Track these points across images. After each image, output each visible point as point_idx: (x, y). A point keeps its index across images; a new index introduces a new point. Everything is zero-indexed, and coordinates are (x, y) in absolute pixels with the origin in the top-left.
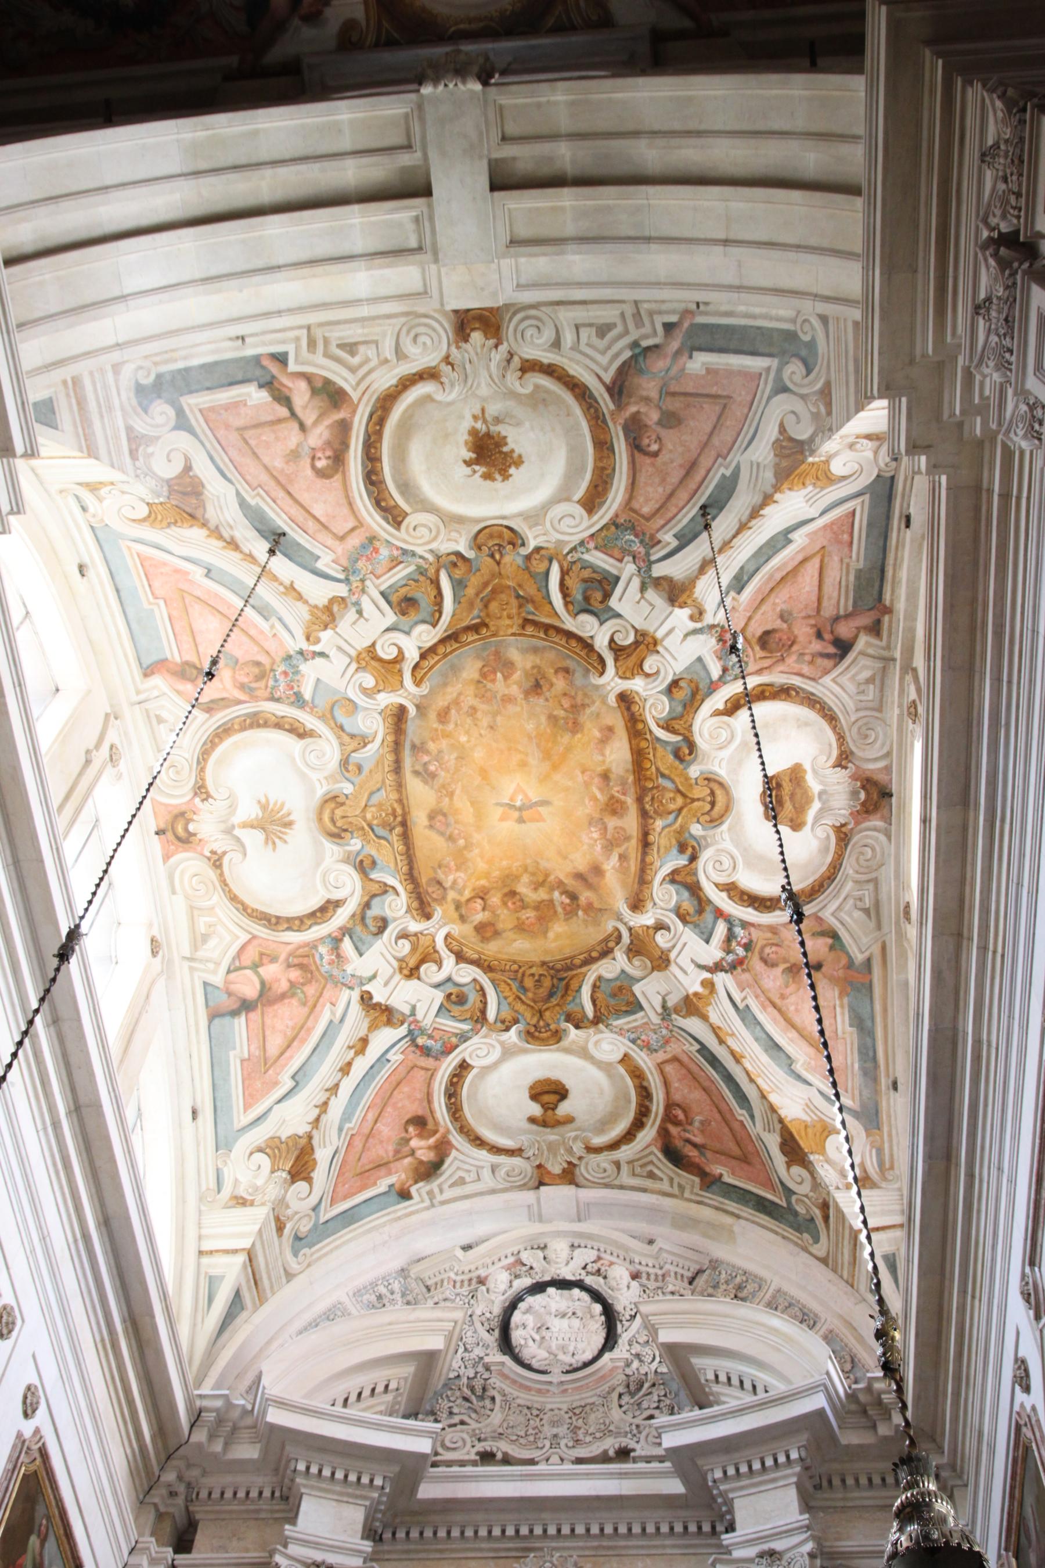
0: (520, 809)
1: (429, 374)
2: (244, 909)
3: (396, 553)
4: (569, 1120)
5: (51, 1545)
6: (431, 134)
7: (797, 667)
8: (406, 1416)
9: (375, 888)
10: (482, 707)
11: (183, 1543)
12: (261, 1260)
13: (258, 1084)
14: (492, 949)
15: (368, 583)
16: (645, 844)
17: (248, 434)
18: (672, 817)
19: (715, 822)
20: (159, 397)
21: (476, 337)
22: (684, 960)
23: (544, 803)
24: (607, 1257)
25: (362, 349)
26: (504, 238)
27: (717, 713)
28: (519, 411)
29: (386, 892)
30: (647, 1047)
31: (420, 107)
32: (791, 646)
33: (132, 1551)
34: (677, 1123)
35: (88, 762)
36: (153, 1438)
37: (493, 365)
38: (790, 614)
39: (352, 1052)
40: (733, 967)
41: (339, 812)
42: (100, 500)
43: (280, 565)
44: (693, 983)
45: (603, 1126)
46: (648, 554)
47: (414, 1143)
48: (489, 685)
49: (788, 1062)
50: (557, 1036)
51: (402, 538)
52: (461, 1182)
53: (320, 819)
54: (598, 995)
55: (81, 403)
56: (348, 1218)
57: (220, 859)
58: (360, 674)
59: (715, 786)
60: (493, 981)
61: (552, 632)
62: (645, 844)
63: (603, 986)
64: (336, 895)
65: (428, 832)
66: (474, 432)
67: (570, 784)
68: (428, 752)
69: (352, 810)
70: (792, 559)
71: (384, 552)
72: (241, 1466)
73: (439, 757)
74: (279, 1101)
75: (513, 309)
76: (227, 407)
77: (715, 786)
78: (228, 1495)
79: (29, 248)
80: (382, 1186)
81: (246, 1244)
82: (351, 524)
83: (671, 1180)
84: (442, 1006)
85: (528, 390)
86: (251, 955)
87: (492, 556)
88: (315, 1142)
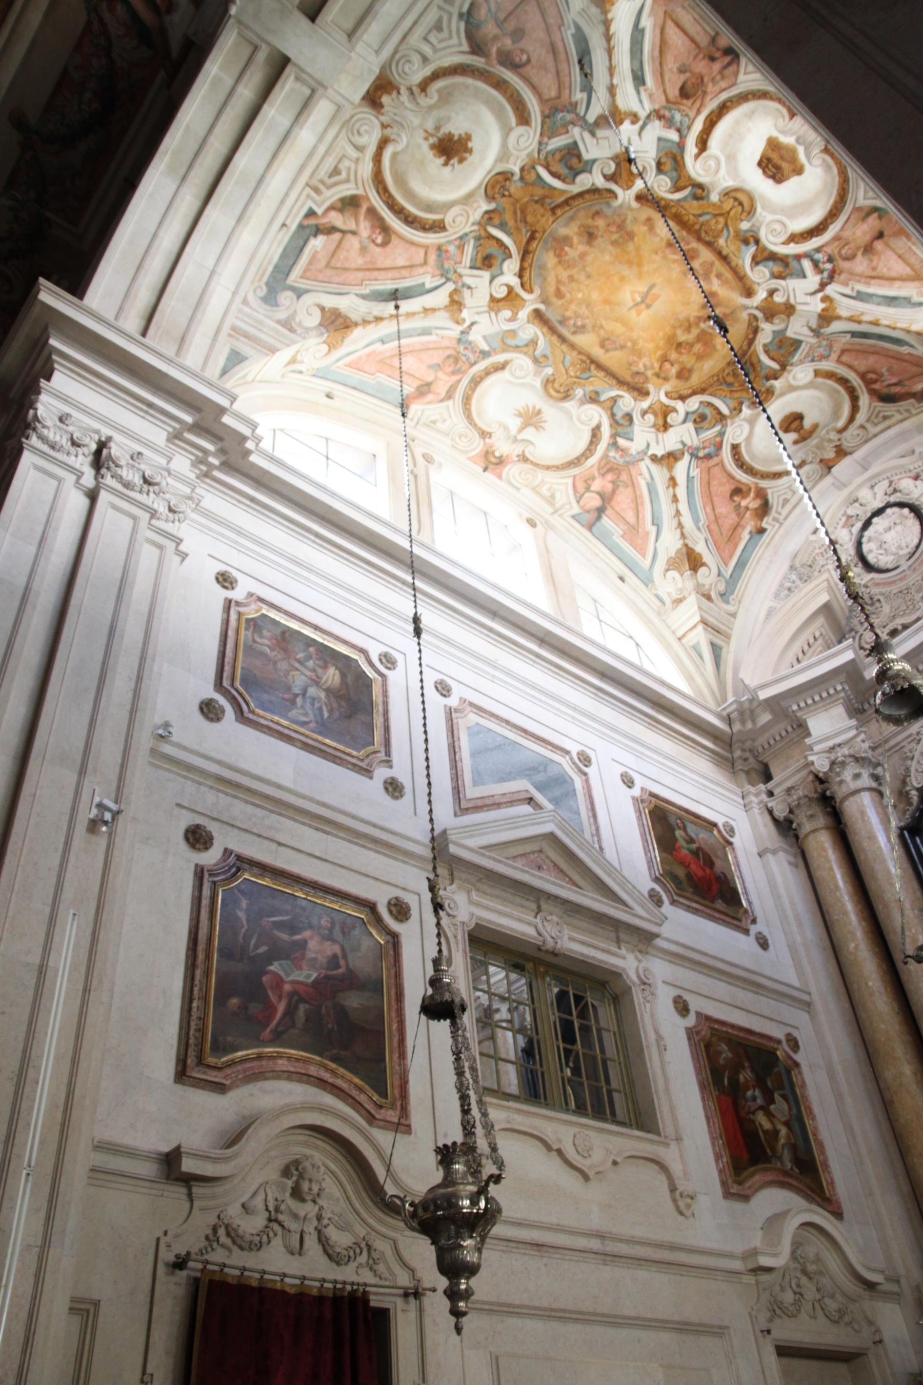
0: (643, 301)
1: (384, 143)
2: (557, 468)
3: (457, 243)
4: (815, 427)
5: (691, 829)
6: (257, 28)
7: (717, 88)
8: (840, 642)
9: (609, 404)
10: (574, 271)
11: (767, 777)
12: (712, 620)
13: (640, 541)
14: (695, 380)
15: (459, 270)
16: (724, 259)
17: (333, 263)
18: (725, 232)
19: (750, 211)
20: (277, 293)
21: (385, 99)
22: (801, 298)
23: (652, 287)
24: (895, 478)
25: (341, 166)
26: (344, 38)
27: (697, 156)
28: (443, 112)
29: (615, 401)
30: (822, 357)
31: (240, 22)
32: (702, 81)
33: (743, 798)
34: (875, 381)
35: (416, 477)
36: (714, 743)
37: (407, 104)
38: (684, 65)
39: (671, 489)
40: (831, 278)
41: (556, 385)
42: (302, 362)
43: (406, 306)
44: (817, 305)
45: (836, 414)
46: (577, 115)
47: (744, 503)
48: (567, 258)
49: (907, 302)
50: (770, 392)
51: (453, 232)
52: (786, 501)
53: (551, 397)
54: (772, 354)
55: (246, 336)
56: (741, 565)
57: (524, 456)
58: (500, 315)
59: (734, 194)
60: (711, 395)
61: (571, 202)
62: (724, 259)
63: (771, 348)
64: (594, 423)
65: (608, 355)
66: (433, 147)
67: (655, 265)
68: (569, 319)
69: (562, 379)
70: (654, 37)
71: (452, 249)
72: (767, 726)
73: (577, 315)
74: (657, 540)
75: (385, 68)
76: (310, 263)
77: (734, 194)
78: (772, 742)
79: (153, 300)
80: (746, 536)
81: (697, 618)
82: (422, 253)
83: (899, 411)
84: (696, 429)
85: (436, 98)
86: (581, 486)
87: (503, 196)
88: (691, 545)
